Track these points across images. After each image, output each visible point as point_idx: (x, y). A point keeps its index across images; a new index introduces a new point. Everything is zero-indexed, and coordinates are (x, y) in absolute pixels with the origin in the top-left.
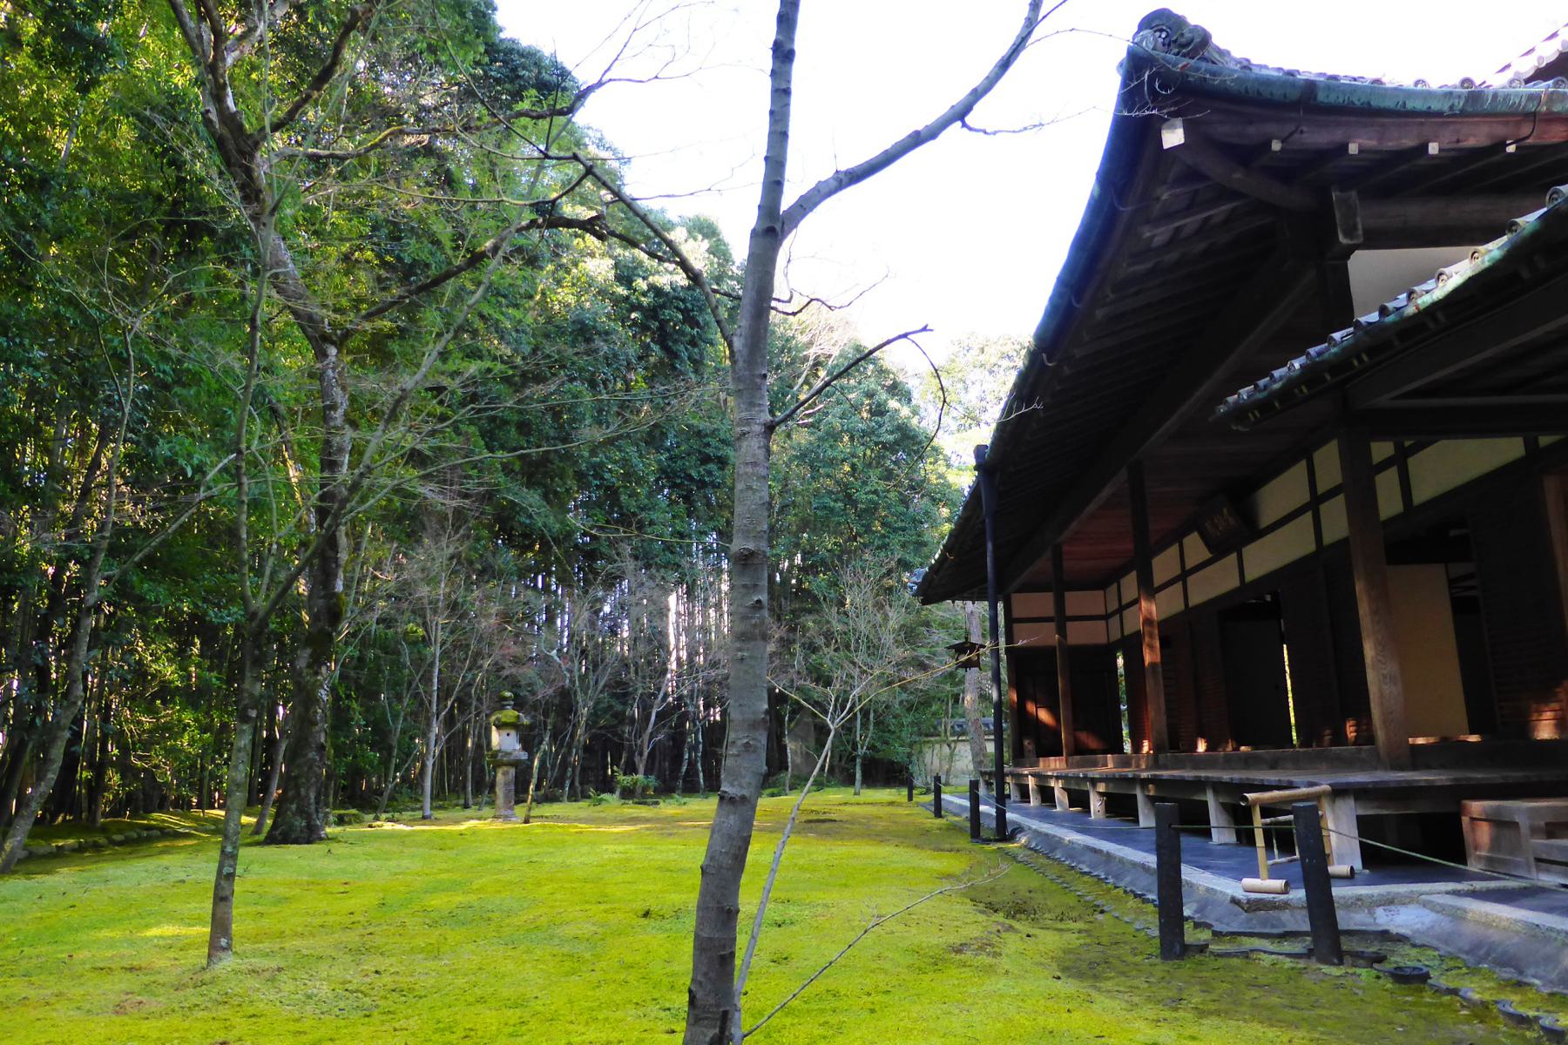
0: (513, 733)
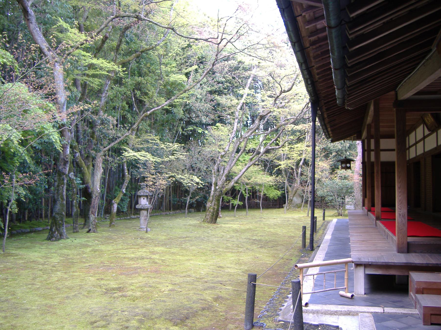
0: (146, 198)
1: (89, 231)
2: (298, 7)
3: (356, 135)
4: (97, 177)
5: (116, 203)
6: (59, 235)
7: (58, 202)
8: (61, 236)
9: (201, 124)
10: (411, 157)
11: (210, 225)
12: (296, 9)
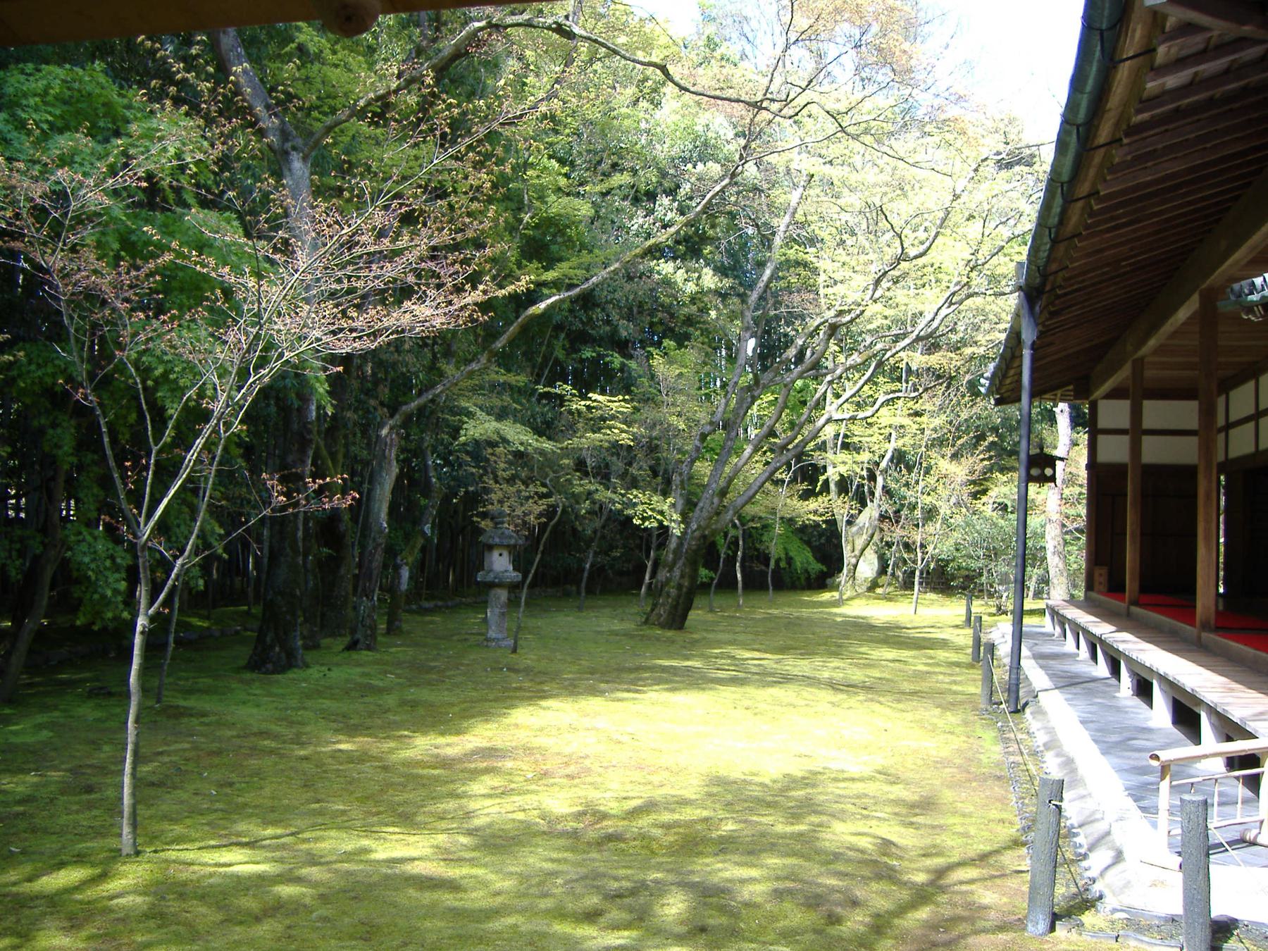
0: (505, 553)
1: (353, 646)
2: (1139, 27)
3: (1071, 387)
4: (382, 489)
5: (407, 564)
6: (283, 655)
7: (282, 559)
8: (289, 662)
9: (623, 347)
10: (1233, 454)
11: (670, 634)
12: (1134, 31)
